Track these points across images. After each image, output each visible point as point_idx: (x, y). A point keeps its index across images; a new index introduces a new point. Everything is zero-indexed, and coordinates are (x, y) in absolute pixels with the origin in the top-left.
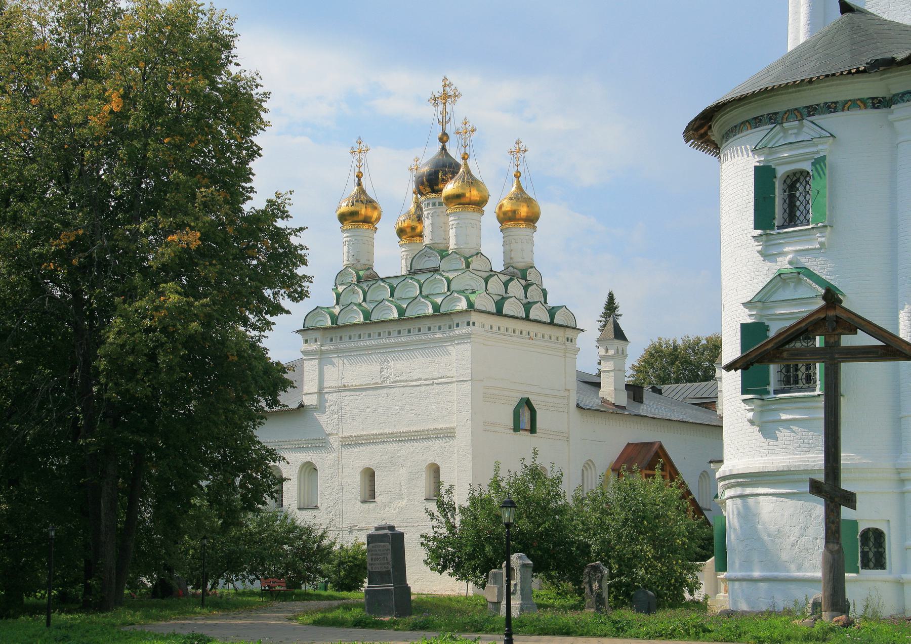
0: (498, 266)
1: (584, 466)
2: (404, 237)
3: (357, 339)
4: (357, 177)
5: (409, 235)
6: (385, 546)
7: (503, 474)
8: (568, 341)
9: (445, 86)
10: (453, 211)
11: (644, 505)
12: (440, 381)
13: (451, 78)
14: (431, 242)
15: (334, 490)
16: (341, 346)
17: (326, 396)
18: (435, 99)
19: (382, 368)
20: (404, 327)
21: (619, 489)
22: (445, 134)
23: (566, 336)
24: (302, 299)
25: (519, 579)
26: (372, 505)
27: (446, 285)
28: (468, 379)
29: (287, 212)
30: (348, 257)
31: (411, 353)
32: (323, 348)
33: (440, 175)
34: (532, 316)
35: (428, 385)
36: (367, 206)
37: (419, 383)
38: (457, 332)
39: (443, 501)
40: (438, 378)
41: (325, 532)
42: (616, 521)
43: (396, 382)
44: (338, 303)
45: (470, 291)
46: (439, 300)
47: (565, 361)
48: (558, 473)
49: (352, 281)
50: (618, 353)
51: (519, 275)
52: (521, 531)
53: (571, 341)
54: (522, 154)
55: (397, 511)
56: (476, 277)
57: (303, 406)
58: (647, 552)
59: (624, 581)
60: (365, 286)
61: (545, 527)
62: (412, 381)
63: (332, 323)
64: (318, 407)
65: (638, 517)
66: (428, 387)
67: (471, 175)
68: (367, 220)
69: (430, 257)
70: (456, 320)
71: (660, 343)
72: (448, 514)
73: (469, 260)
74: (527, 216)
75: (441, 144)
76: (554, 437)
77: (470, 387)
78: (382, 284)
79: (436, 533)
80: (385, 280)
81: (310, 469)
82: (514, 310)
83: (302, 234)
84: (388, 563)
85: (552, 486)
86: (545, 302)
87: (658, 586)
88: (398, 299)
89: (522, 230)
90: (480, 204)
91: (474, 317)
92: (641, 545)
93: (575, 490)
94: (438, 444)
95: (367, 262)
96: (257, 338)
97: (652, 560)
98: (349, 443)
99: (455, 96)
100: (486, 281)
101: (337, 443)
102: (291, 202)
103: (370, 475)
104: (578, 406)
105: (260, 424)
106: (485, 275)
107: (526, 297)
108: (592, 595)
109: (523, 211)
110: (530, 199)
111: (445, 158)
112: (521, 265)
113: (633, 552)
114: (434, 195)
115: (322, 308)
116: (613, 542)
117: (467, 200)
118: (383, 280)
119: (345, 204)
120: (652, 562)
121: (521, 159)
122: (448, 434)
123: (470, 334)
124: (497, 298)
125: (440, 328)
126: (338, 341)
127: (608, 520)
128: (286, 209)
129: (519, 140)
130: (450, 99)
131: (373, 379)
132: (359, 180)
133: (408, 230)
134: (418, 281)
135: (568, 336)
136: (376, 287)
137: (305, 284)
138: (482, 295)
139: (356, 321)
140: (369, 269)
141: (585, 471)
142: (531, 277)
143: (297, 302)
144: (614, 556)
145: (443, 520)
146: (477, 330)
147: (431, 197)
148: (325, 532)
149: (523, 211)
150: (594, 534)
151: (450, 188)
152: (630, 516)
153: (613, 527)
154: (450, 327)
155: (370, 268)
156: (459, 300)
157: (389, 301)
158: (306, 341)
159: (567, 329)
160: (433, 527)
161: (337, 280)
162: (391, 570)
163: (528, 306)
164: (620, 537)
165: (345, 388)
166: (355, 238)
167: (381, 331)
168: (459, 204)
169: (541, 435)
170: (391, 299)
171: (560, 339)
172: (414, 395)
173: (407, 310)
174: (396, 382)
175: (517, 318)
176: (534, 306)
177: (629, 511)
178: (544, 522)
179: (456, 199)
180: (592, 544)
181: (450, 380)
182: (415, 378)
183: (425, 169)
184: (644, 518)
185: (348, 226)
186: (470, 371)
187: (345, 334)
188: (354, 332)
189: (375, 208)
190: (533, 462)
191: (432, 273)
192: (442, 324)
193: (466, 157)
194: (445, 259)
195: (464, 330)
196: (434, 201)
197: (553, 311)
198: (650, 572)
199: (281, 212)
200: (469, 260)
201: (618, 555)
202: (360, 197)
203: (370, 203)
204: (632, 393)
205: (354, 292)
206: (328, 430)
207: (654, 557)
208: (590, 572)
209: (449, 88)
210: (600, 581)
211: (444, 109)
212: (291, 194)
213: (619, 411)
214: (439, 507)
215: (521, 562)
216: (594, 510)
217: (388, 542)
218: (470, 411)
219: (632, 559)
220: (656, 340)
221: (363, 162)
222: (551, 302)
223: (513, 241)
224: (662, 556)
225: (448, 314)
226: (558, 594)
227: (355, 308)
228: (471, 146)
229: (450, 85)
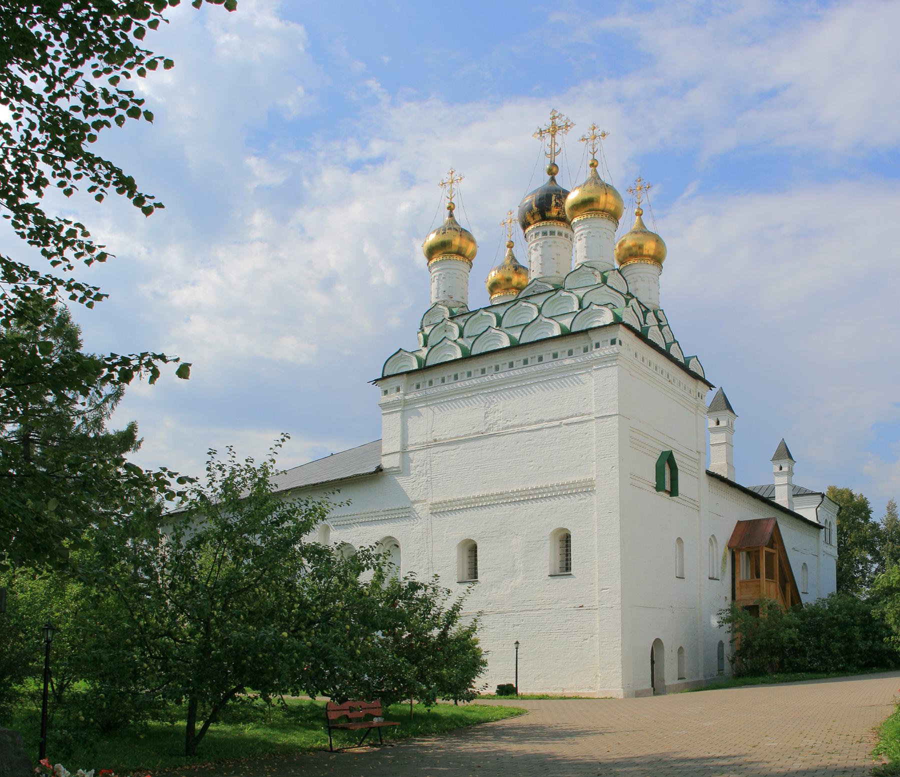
3: (452, 380)
5: (503, 287)
9: (554, 118)
13: (561, 110)
14: (541, 276)
15: (422, 570)
16: (432, 391)
17: (411, 455)
19: (487, 413)
28: (614, 413)
30: (438, 294)
31: (527, 390)
32: (407, 397)
35: (554, 427)
37: (539, 426)
38: (597, 353)
40: (568, 418)
41: (457, 608)
43: (508, 427)
44: (425, 345)
55: (508, 592)
57: (381, 470)
62: (530, 425)
64: (401, 469)
66: (554, 430)
70: (595, 337)
75: (549, 177)
77: (616, 425)
95: (461, 300)
99: (567, 126)
101: (425, 512)
114: (545, 222)
117: (601, 207)
122: (586, 488)
123: (617, 354)
129: (640, 178)
131: (474, 428)
135: (700, 391)
148: (457, 608)
149: (650, 247)
156: (600, 313)
158: (386, 392)
161: (424, 321)
165: (436, 443)
166: (447, 271)
168: (590, 210)
172: (533, 442)
174: (508, 427)
181: (586, 418)
182: (535, 419)
186: (616, 402)
187: (436, 375)
192: (573, 348)
193: (595, 164)
195: (607, 350)
196: (544, 230)
203: (463, 233)
206: (413, 496)
209: (559, 119)
218: (617, 456)
223: (639, 279)
229: (561, 115)
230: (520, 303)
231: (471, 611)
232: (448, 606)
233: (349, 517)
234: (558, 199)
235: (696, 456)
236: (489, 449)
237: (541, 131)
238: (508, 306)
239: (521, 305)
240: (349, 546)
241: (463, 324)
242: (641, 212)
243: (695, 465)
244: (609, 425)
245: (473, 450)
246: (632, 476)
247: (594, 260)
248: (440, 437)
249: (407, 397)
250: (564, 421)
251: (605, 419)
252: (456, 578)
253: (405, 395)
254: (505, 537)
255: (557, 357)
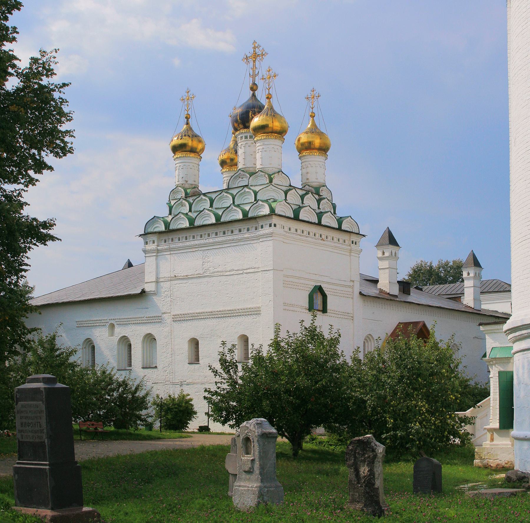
0: (297, 182)
1: (365, 339)
2: (225, 166)
4: (186, 118)
6: (37, 406)
7: (283, 335)
8: (352, 243)
9: (254, 48)
10: (259, 139)
11: (419, 363)
12: (248, 271)
14: (244, 167)
17: (162, 284)
18: (247, 58)
19: (203, 262)
20: (221, 229)
21: (395, 348)
22: (254, 84)
23: (351, 240)
24: (65, 155)
25: (257, 453)
26: (196, 366)
27: (254, 196)
29: (52, 70)
32: (159, 248)
33: (250, 115)
34: (323, 223)
36: (193, 139)
38: (261, 232)
39: (226, 360)
42: (392, 378)
43: (214, 272)
44: (170, 214)
45: (272, 200)
46: (247, 208)
47: (350, 258)
48: (336, 334)
49: (182, 197)
50: (392, 255)
51: (314, 192)
52: (297, 388)
53: (356, 244)
54: (316, 99)
56: (278, 189)
57: (145, 292)
58: (422, 406)
59: (399, 434)
60: (191, 200)
61: (322, 384)
63: (166, 228)
65: (413, 374)
67: (274, 111)
68: (193, 150)
69: (242, 178)
71: (421, 264)
72: (231, 371)
73: (272, 176)
74: (320, 146)
76: (342, 316)
78: (204, 198)
79: (219, 388)
80: (207, 195)
81: (150, 339)
82: (309, 217)
83: (65, 89)
84: (42, 431)
85: (331, 347)
86: (335, 213)
87: (431, 438)
88: (216, 208)
89: (315, 158)
90: (281, 133)
91: (275, 220)
92: (415, 400)
93: (353, 352)
94: (248, 320)
95: (193, 183)
96: (18, 192)
97: (426, 414)
98: (179, 319)
99: (263, 55)
100: (286, 193)
101: (170, 320)
102: (56, 60)
103: (195, 343)
104: (361, 293)
105: (22, 278)
106: (285, 189)
107: (319, 208)
108: (358, 483)
109: (317, 142)
110: (322, 133)
111: (254, 102)
112: (315, 184)
113: (408, 407)
115: (158, 217)
116: (389, 398)
117: (270, 130)
118: (204, 194)
119: (176, 138)
120: (426, 416)
121: (315, 103)
122: (256, 312)
123: (272, 233)
124: (295, 207)
125: (248, 230)
126: (170, 242)
127: (383, 378)
128: (51, 68)
129: (313, 89)
130: (258, 58)
131: (196, 271)
132: (188, 120)
133: (228, 161)
134: (232, 194)
135: (353, 240)
136: (199, 200)
137: (67, 139)
138: (282, 203)
139: (183, 226)
140: (195, 188)
141: (366, 342)
142: (324, 193)
143: (60, 158)
144: (389, 411)
145: (225, 376)
146: (278, 230)
147: (243, 132)
149: (317, 142)
150: (371, 390)
151: (256, 121)
152: (406, 373)
153: (389, 384)
154: (256, 229)
155: (196, 187)
157: (208, 210)
158: (146, 243)
159: (352, 234)
160: (216, 382)
161: (171, 196)
162: (46, 441)
163: (320, 215)
164: (395, 393)
165: (176, 278)
166: (184, 164)
167: (203, 233)
169: (331, 315)
170: (210, 209)
171: (347, 241)
173: (223, 217)
174: (214, 272)
175: (311, 223)
176: (325, 215)
177: (404, 369)
178: (321, 380)
179: (262, 129)
180: (368, 400)
181: (256, 270)
182: (229, 269)
183: (239, 111)
184: (419, 375)
185: (179, 155)
186: (272, 262)
187: (175, 236)
188: (183, 235)
189: (200, 141)
190: (312, 324)
191: (243, 188)
194: (253, 176)
195: (267, 230)
196: (246, 135)
197: (341, 220)
198: (424, 425)
199: (47, 70)
200: (272, 176)
201: (393, 409)
202: (188, 133)
203: (194, 136)
204: (402, 287)
205: (182, 205)
207: (427, 411)
208: (356, 449)
210: (371, 463)
211: (254, 65)
212: (56, 52)
213: (392, 298)
214: (221, 364)
215: (260, 430)
216: (371, 369)
217: (42, 400)
219: (407, 413)
220: (419, 262)
221: (190, 106)
222: (339, 214)
223: (309, 166)
224: (437, 410)
225: (254, 218)
226: (339, 440)
227: (182, 216)
228: (274, 88)
229: (259, 46)
230: (224, 193)
231: (195, 381)
232: (136, 384)
233: (130, 320)
234: (253, 114)
235: (351, 284)
236: (205, 284)
237: (247, 57)
238: (219, 193)
239: (224, 195)
240: (127, 338)
241: (192, 202)
242: (313, 115)
243: (350, 290)
244: (268, 275)
245: (196, 284)
246: (284, 304)
247: (266, 167)
248: (177, 274)
249: (159, 248)
250: (245, 271)
251: (266, 272)
252: (187, 361)
253: (158, 246)
254: (214, 338)
255: (241, 232)
